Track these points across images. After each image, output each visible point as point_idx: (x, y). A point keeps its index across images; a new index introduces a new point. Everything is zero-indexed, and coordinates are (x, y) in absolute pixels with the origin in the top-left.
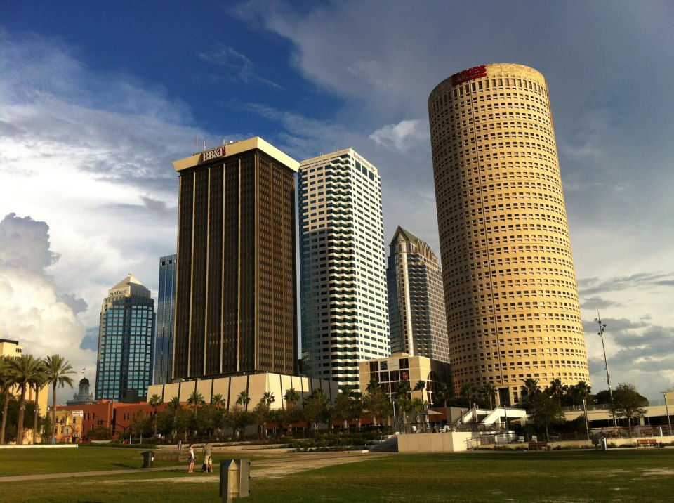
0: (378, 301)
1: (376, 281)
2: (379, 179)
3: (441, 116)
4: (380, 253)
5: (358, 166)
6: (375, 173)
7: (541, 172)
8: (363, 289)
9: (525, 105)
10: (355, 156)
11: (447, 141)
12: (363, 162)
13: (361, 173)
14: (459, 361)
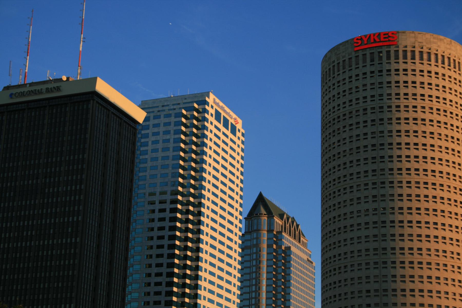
0: (229, 247)
1: (228, 273)
2: (243, 135)
3: (336, 85)
4: (237, 202)
5: (218, 116)
6: (239, 126)
7: (452, 171)
8: (212, 237)
9: (441, 86)
10: (215, 102)
11: (342, 118)
12: (225, 111)
13: (221, 126)
14: (333, 299)
